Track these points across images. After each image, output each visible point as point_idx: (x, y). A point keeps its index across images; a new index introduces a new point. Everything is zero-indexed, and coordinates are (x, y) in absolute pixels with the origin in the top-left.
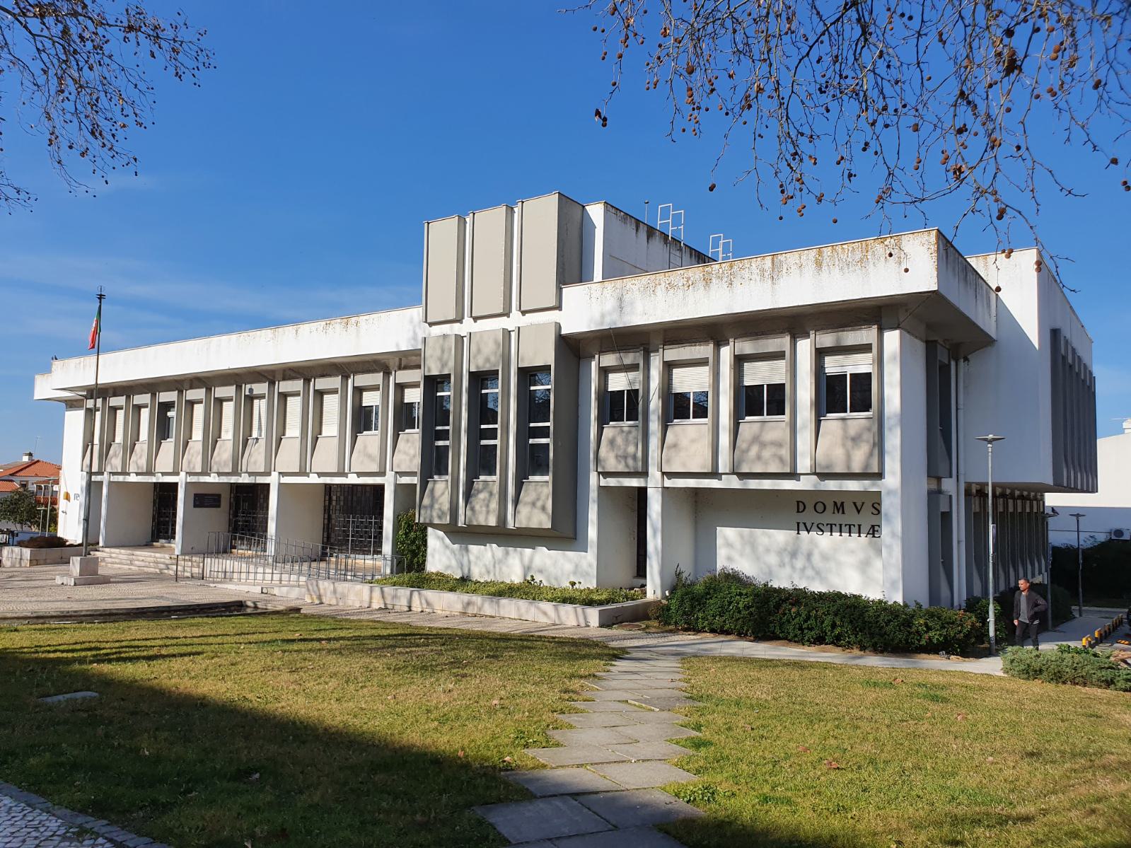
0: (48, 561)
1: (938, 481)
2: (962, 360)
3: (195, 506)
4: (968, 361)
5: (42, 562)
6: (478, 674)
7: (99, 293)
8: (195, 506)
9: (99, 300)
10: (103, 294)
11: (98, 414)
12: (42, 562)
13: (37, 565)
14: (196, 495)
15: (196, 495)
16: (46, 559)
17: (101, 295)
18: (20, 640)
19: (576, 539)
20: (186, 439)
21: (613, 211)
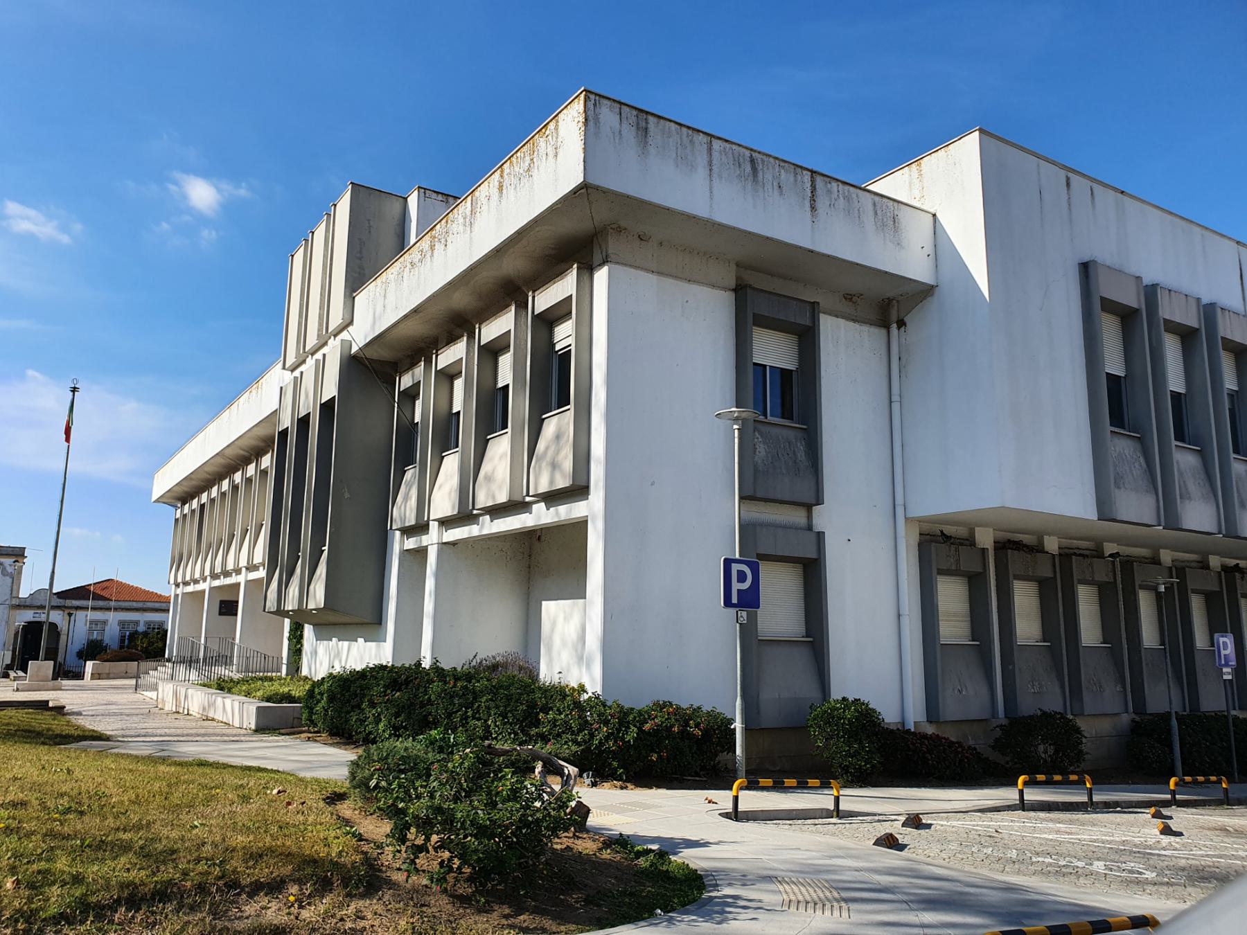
0: (111, 676)
1: (808, 509)
2: (895, 325)
3: (221, 614)
4: (906, 326)
5: (105, 676)
6: (1154, 758)
7: (73, 386)
8: (221, 614)
9: (72, 393)
10: (76, 386)
11: (459, 384)
12: (105, 676)
13: (99, 679)
14: (222, 602)
15: (222, 602)
16: (109, 674)
17: (75, 388)
18: (1238, 790)
19: (381, 624)
20: (245, 527)
21: (440, 197)
